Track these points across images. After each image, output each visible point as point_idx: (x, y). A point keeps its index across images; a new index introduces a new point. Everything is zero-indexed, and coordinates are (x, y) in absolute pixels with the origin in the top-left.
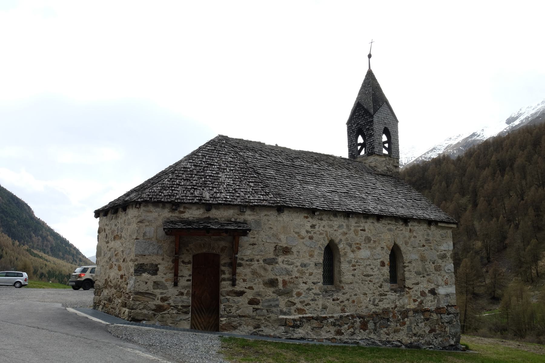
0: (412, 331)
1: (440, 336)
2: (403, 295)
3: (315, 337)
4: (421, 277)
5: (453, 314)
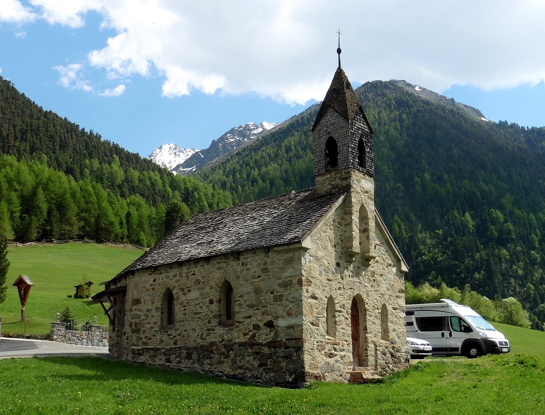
0: (236, 363)
1: (272, 371)
2: (232, 330)
3: (152, 363)
4: (255, 310)
5: (294, 348)
